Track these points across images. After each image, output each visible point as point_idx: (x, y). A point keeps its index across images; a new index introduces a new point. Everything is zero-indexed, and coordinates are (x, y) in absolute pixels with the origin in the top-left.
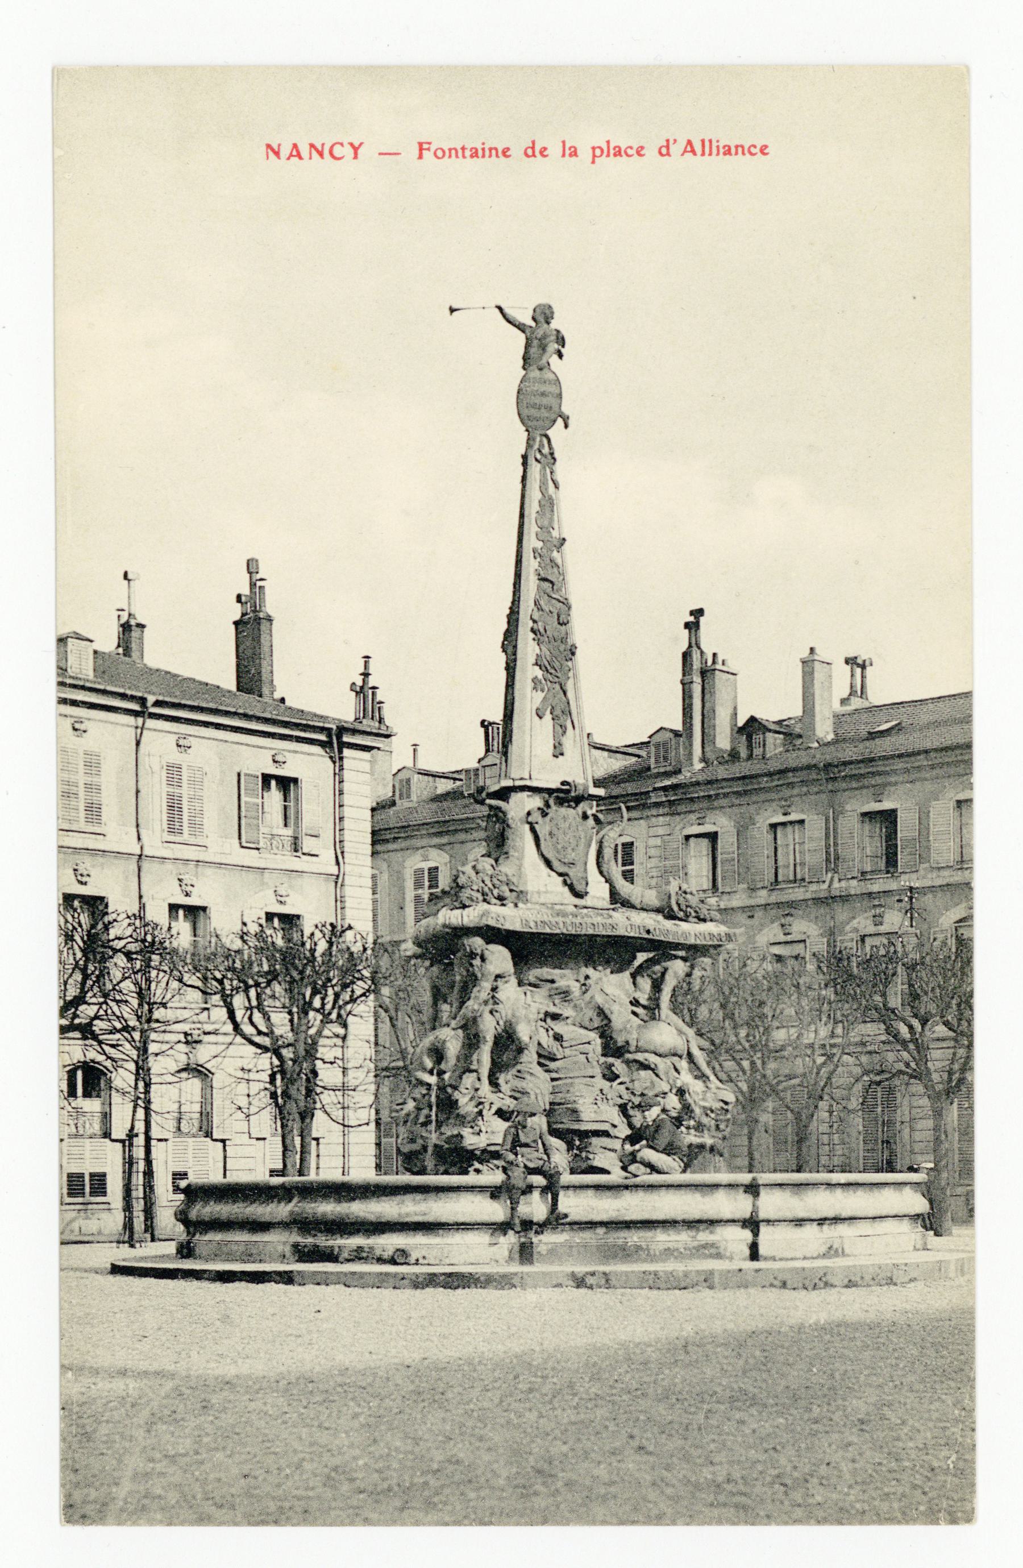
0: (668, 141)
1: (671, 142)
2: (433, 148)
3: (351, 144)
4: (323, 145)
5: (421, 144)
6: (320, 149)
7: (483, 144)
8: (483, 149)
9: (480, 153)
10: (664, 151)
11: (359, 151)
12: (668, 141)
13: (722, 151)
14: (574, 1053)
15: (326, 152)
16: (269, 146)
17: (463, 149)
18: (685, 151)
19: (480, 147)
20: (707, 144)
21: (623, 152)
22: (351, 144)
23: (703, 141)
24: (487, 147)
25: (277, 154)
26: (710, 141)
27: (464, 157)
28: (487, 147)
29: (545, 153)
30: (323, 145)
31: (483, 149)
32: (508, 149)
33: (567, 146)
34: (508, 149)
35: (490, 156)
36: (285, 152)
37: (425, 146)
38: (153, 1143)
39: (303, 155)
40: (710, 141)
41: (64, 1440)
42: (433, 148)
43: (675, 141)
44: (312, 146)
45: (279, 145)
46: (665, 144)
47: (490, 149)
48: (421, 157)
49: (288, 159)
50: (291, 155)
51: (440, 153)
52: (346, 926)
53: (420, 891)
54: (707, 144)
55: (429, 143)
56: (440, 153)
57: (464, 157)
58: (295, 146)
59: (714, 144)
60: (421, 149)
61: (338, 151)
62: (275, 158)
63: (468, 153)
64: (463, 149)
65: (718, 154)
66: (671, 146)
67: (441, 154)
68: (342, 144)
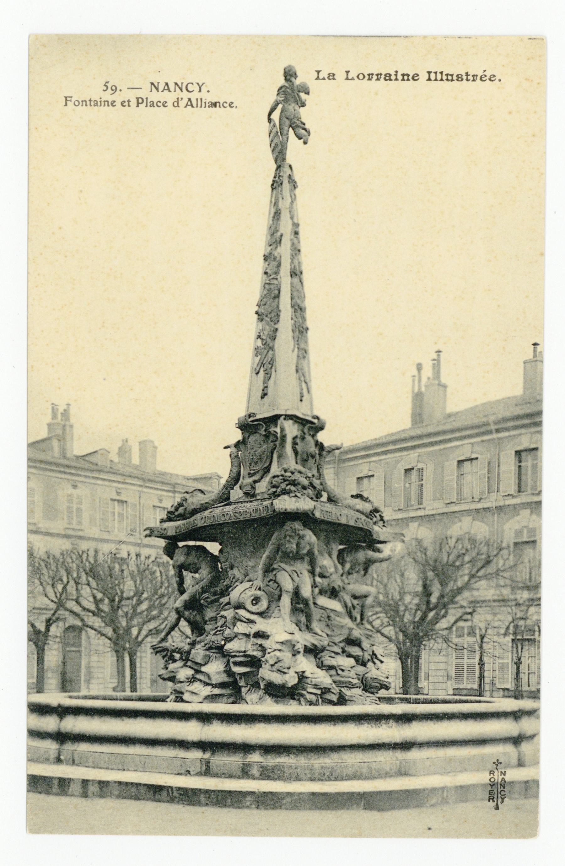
0: (178, 98)
1: (180, 99)
2: (73, 100)
3: (198, 84)
4: (182, 83)
5: (66, 98)
6: (181, 86)
7: (101, 98)
8: (101, 102)
9: (393, 77)
10: (176, 104)
11: (202, 88)
12: (178, 98)
13: (207, 105)
14: (163, 626)
15: (184, 89)
16: (152, 84)
17: (90, 100)
18: (187, 105)
19: (393, 73)
20: (199, 101)
21: (155, 105)
22: (198, 84)
23: (197, 99)
24: (103, 100)
25: (157, 89)
26: (201, 99)
27: (91, 105)
28: (103, 100)
29: (114, 104)
30: (182, 83)
31: (101, 102)
32: (114, 101)
33: (149, 101)
34: (114, 101)
35: (104, 105)
36: (161, 88)
37: (68, 99)
38: (176, 629)
39: (171, 90)
40: (201, 99)
41: (61, 833)
42: (73, 100)
43: (182, 99)
44: (176, 84)
45: (158, 83)
46: (176, 100)
47: (104, 101)
48: (66, 105)
49: (163, 91)
50: (164, 89)
51: (77, 103)
52: (81, 553)
53: (492, 424)
54: (199, 101)
55: (71, 97)
56: (77, 103)
57: (91, 105)
58: (167, 84)
59: (204, 101)
60: (66, 100)
61: (190, 88)
62: (156, 91)
63: (92, 103)
64: (90, 100)
65: (205, 107)
66: (180, 102)
67: (77, 104)
68: (192, 84)
